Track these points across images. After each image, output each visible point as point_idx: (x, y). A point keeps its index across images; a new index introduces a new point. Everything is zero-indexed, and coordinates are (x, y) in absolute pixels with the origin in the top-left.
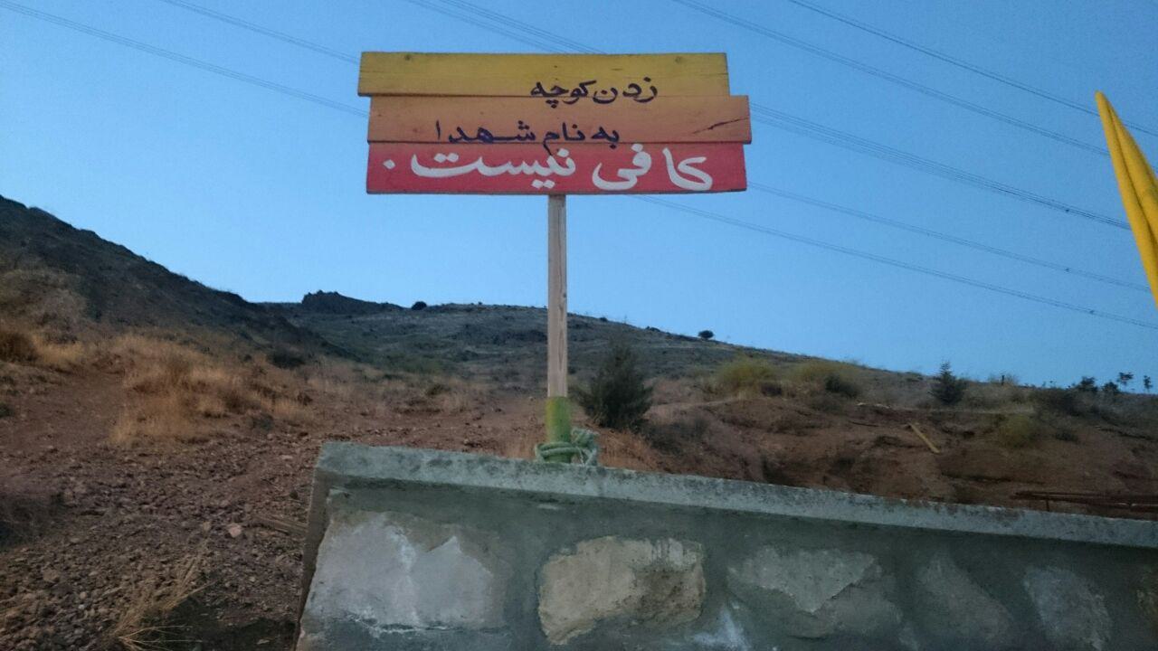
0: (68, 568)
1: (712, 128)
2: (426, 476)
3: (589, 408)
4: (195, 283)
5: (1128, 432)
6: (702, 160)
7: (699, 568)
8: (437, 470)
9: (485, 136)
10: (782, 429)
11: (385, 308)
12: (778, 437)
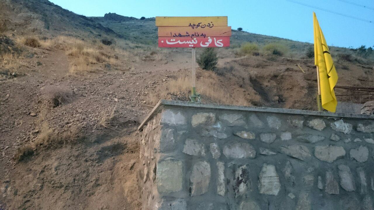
0: (83, 109)
1: (224, 33)
2: (175, 104)
3: (199, 64)
4: (71, 12)
5: (365, 67)
6: (221, 40)
7: (215, 117)
8: (177, 103)
9: (180, 36)
10: (258, 67)
11: (132, 19)
12: (256, 69)
